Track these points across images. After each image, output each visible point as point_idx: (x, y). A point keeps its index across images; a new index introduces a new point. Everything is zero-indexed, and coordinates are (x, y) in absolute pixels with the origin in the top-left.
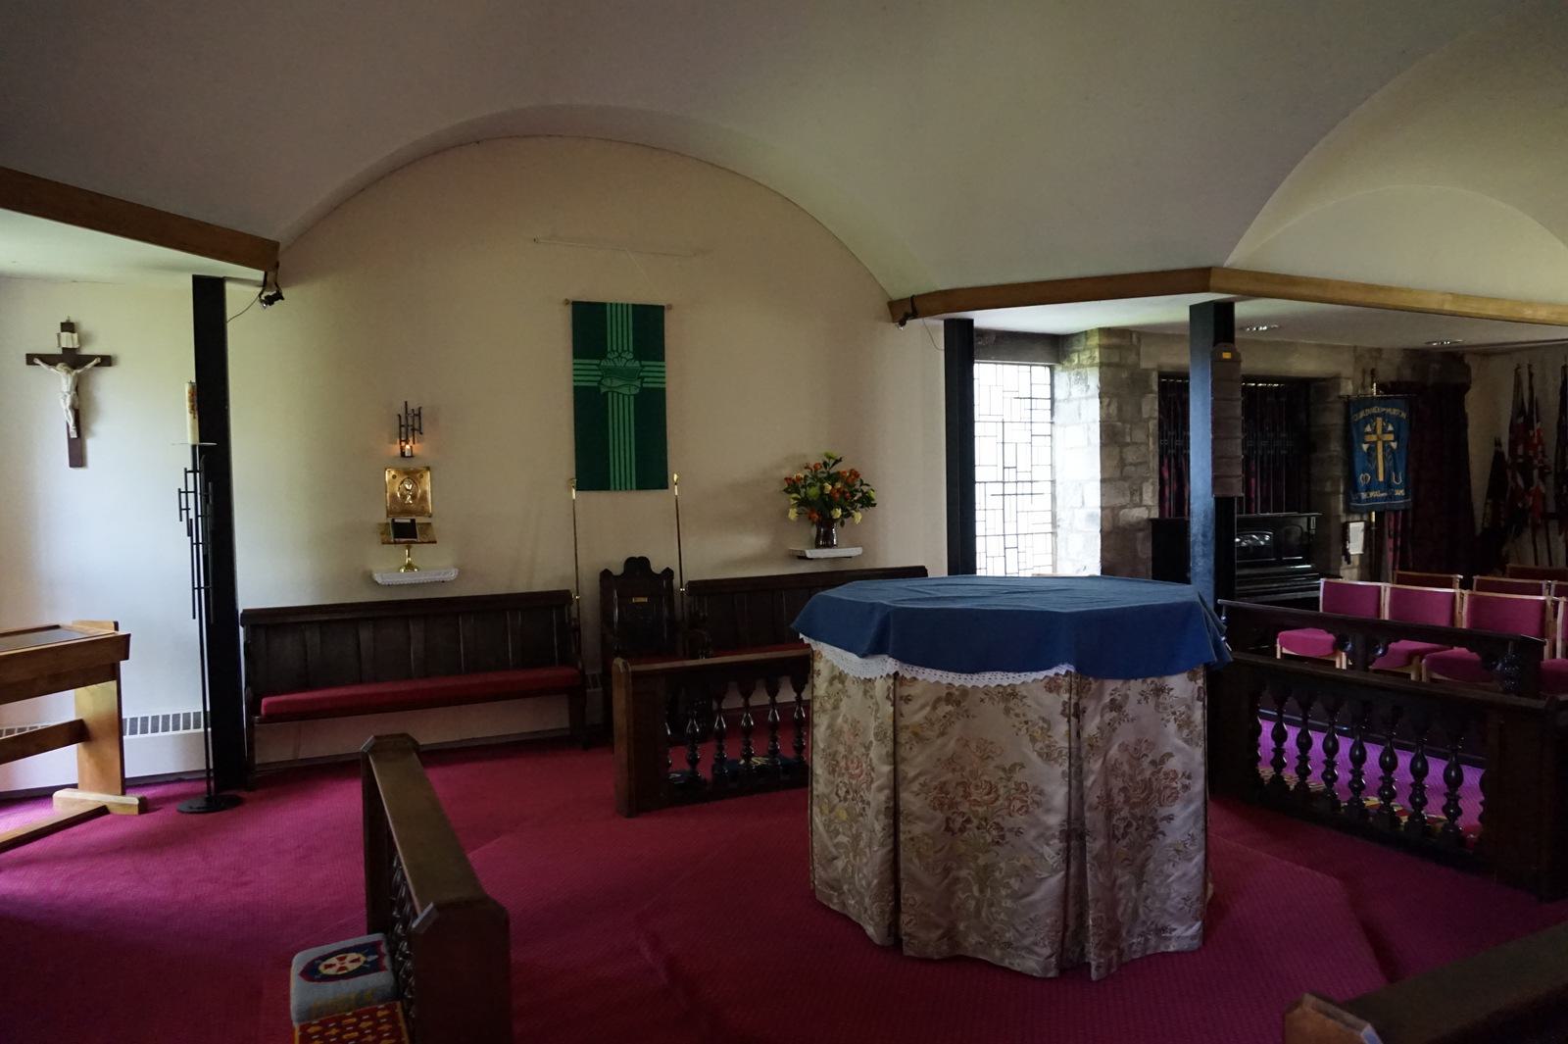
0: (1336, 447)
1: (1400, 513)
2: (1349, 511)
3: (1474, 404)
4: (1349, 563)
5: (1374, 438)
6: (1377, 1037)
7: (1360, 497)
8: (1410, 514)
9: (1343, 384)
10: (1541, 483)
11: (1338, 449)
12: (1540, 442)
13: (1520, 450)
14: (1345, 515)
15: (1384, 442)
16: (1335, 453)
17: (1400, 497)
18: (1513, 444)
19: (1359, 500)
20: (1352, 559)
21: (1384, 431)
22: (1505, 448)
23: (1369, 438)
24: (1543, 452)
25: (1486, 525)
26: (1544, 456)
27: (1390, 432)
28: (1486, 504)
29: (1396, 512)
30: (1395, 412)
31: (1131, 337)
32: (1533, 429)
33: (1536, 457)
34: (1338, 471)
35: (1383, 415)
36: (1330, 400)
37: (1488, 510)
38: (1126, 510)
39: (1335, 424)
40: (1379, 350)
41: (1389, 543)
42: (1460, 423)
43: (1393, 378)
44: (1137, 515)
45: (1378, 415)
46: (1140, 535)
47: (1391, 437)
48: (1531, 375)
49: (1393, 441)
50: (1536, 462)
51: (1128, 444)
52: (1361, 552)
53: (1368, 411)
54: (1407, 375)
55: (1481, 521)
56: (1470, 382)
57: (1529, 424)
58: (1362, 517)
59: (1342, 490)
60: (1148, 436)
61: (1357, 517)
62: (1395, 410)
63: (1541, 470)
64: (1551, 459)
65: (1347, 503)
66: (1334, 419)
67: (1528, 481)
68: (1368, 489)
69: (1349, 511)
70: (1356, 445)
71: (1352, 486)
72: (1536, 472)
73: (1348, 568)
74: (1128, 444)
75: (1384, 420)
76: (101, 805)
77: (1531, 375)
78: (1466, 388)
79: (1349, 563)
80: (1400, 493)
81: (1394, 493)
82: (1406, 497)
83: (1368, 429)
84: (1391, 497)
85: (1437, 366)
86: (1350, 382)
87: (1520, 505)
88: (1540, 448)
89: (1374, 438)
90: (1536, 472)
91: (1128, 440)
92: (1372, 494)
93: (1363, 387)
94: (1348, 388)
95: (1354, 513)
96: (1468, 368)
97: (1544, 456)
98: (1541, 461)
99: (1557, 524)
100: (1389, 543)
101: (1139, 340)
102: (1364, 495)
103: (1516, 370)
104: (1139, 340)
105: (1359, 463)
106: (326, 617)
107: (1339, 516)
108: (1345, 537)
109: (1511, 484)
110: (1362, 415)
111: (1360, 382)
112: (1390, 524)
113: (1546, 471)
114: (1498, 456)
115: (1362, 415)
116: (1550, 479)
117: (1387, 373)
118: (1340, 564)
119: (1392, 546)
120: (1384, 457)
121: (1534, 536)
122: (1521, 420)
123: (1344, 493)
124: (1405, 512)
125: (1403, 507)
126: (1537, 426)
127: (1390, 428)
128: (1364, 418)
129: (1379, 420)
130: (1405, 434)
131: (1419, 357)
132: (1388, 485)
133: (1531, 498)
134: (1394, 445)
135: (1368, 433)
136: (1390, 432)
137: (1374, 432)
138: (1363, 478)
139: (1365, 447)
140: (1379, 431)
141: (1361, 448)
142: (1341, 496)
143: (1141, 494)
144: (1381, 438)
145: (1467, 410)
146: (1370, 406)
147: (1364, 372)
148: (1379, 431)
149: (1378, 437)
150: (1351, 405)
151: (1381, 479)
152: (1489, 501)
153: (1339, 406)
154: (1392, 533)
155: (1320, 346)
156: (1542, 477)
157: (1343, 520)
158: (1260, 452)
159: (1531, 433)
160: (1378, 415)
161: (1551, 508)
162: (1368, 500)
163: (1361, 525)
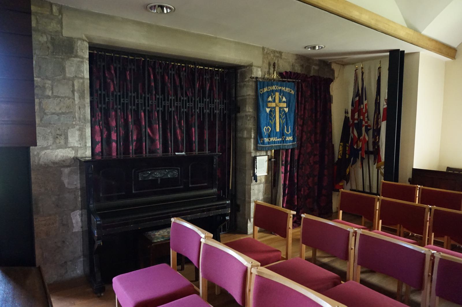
0: (249, 109)
1: (290, 150)
2: (257, 149)
3: (335, 90)
4: (256, 181)
5: (273, 105)
6: (317, 252)
7: (263, 141)
8: (296, 152)
9: (255, 70)
10: (366, 135)
11: (251, 110)
12: (367, 111)
13: (356, 116)
14: (254, 152)
15: (280, 108)
16: (249, 113)
17: (290, 141)
18: (353, 112)
19: (263, 143)
20: (258, 178)
21: (280, 101)
22: (349, 115)
23: (270, 105)
24: (367, 117)
25: (340, 157)
26: (368, 120)
27: (284, 102)
28: (340, 145)
29: (287, 150)
30: (287, 90)
31: (52, 9)
32: (363, 104)
33: (364, 119)
34: (250, 124)
35: (280, 91)
36: (247, 79)
37: (341, 149)
38: (48, 151)
39: (249, 95)
40: (280, 53)
41: (282, 169)
42: (328, 100)
43: (289, 69)
44: (62, 154)
45: (276, 91)
46: (66, 171)
47: (285, 105)
48: (363, 73)
49: (286, 107)
50: (364, 122)
51: (48, 97)
52: (266, 174)
53: (271, 88)
54: (298, 69)
55: (337, 155)
56: (334, 79)
57: (361, 102)
58: (267, 153)
59: (253, 137)
60: (73, 91)
61: (264, 153)
62: (287, 89)
63: (366, 127)
64: (371, 122)
65: (256, 143)
66: (248, 92)
67: (360, 134)
68: (269, 136)
69: (257, 149)
70: (261, 109)
71: (259, 134)
72: (364, 128)
73: (256, 184)
74: (48, 97)
75: (280, 94)
76: (383, 109)
77: (363, 73)
78: (331, 80)
79: (256, 181)
80: (290, 138)
81: (285, 138)
82: (293, 141)
83: (270, 99)
84: (284, 141)
85: (316, 68)
86: (259, 69)
87: (355, 147)
88: (366, 115)
89: (273, 105)
90: (364, 128)
91: (50, 94)
92: (272, 139)
93: (269, 73)
94: (258, 73)
95: (261, 150)
96: (333, 71)
97: (368, 120)
98: (366, 122)
99: (373, 157)
100: (282, 169)
101: (60, 13)
102: (266, 140)
103: (355, 71)
104: (60, 13)
105: (263, 121)
106: (206, 132)
107: (251, 153)
108: (254, 166)
109: (352, 135)
110: (266, 90)
111: (267, 70)
112: (282, 157)
113: (369, 128)
114: (346, 119)
115: (266, 90)
116: (371, 132)
117: (285, 66)
118: (252, 182)
119: (283, 171)
120: (280, 117)
121: (362, 164)
122: (357, 99)
123: (254, 139)
124: (293, 150)
125: (291, 147)
126: (365, 102)
127: (284, 99)
128: (267, 92)
129: (277, 94)
130: (294, 104)
131: (305, 60)
132: (282, 134)
133: (361, 143)
134: (286, 110)
135: (270, 102)
136: (284, 102)
137: (274, 101)
138: (265, 130)
139: (268, 110)
140: (277, 101)
141: (266, 112)
142: (252, 140)
143: (66, 138)
144: (278, 105)
145: (331, 93)
146: (272, 85)
147: (269, 64)
148: (277, 101)
149: (276, 105)
150: (259, 83)
151: (278, 130)
152: (342, 144)
153: (252, 84)
154: (284, 163)
155: (236, 43)
156: (367, 131)
157: (253, 155)
158: (198, 110)
159: (362, 107)
160: (276, 91)
161: (371, 149)
162: (269, 143)
163: (266, 158)
